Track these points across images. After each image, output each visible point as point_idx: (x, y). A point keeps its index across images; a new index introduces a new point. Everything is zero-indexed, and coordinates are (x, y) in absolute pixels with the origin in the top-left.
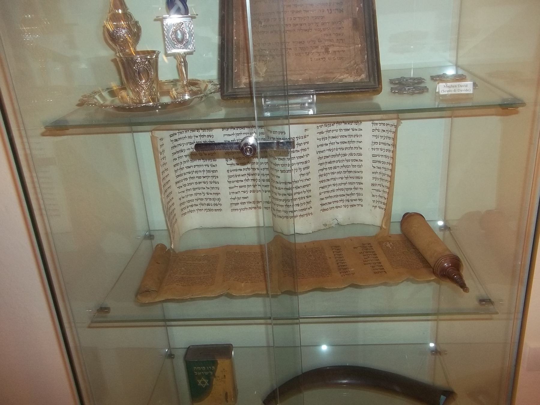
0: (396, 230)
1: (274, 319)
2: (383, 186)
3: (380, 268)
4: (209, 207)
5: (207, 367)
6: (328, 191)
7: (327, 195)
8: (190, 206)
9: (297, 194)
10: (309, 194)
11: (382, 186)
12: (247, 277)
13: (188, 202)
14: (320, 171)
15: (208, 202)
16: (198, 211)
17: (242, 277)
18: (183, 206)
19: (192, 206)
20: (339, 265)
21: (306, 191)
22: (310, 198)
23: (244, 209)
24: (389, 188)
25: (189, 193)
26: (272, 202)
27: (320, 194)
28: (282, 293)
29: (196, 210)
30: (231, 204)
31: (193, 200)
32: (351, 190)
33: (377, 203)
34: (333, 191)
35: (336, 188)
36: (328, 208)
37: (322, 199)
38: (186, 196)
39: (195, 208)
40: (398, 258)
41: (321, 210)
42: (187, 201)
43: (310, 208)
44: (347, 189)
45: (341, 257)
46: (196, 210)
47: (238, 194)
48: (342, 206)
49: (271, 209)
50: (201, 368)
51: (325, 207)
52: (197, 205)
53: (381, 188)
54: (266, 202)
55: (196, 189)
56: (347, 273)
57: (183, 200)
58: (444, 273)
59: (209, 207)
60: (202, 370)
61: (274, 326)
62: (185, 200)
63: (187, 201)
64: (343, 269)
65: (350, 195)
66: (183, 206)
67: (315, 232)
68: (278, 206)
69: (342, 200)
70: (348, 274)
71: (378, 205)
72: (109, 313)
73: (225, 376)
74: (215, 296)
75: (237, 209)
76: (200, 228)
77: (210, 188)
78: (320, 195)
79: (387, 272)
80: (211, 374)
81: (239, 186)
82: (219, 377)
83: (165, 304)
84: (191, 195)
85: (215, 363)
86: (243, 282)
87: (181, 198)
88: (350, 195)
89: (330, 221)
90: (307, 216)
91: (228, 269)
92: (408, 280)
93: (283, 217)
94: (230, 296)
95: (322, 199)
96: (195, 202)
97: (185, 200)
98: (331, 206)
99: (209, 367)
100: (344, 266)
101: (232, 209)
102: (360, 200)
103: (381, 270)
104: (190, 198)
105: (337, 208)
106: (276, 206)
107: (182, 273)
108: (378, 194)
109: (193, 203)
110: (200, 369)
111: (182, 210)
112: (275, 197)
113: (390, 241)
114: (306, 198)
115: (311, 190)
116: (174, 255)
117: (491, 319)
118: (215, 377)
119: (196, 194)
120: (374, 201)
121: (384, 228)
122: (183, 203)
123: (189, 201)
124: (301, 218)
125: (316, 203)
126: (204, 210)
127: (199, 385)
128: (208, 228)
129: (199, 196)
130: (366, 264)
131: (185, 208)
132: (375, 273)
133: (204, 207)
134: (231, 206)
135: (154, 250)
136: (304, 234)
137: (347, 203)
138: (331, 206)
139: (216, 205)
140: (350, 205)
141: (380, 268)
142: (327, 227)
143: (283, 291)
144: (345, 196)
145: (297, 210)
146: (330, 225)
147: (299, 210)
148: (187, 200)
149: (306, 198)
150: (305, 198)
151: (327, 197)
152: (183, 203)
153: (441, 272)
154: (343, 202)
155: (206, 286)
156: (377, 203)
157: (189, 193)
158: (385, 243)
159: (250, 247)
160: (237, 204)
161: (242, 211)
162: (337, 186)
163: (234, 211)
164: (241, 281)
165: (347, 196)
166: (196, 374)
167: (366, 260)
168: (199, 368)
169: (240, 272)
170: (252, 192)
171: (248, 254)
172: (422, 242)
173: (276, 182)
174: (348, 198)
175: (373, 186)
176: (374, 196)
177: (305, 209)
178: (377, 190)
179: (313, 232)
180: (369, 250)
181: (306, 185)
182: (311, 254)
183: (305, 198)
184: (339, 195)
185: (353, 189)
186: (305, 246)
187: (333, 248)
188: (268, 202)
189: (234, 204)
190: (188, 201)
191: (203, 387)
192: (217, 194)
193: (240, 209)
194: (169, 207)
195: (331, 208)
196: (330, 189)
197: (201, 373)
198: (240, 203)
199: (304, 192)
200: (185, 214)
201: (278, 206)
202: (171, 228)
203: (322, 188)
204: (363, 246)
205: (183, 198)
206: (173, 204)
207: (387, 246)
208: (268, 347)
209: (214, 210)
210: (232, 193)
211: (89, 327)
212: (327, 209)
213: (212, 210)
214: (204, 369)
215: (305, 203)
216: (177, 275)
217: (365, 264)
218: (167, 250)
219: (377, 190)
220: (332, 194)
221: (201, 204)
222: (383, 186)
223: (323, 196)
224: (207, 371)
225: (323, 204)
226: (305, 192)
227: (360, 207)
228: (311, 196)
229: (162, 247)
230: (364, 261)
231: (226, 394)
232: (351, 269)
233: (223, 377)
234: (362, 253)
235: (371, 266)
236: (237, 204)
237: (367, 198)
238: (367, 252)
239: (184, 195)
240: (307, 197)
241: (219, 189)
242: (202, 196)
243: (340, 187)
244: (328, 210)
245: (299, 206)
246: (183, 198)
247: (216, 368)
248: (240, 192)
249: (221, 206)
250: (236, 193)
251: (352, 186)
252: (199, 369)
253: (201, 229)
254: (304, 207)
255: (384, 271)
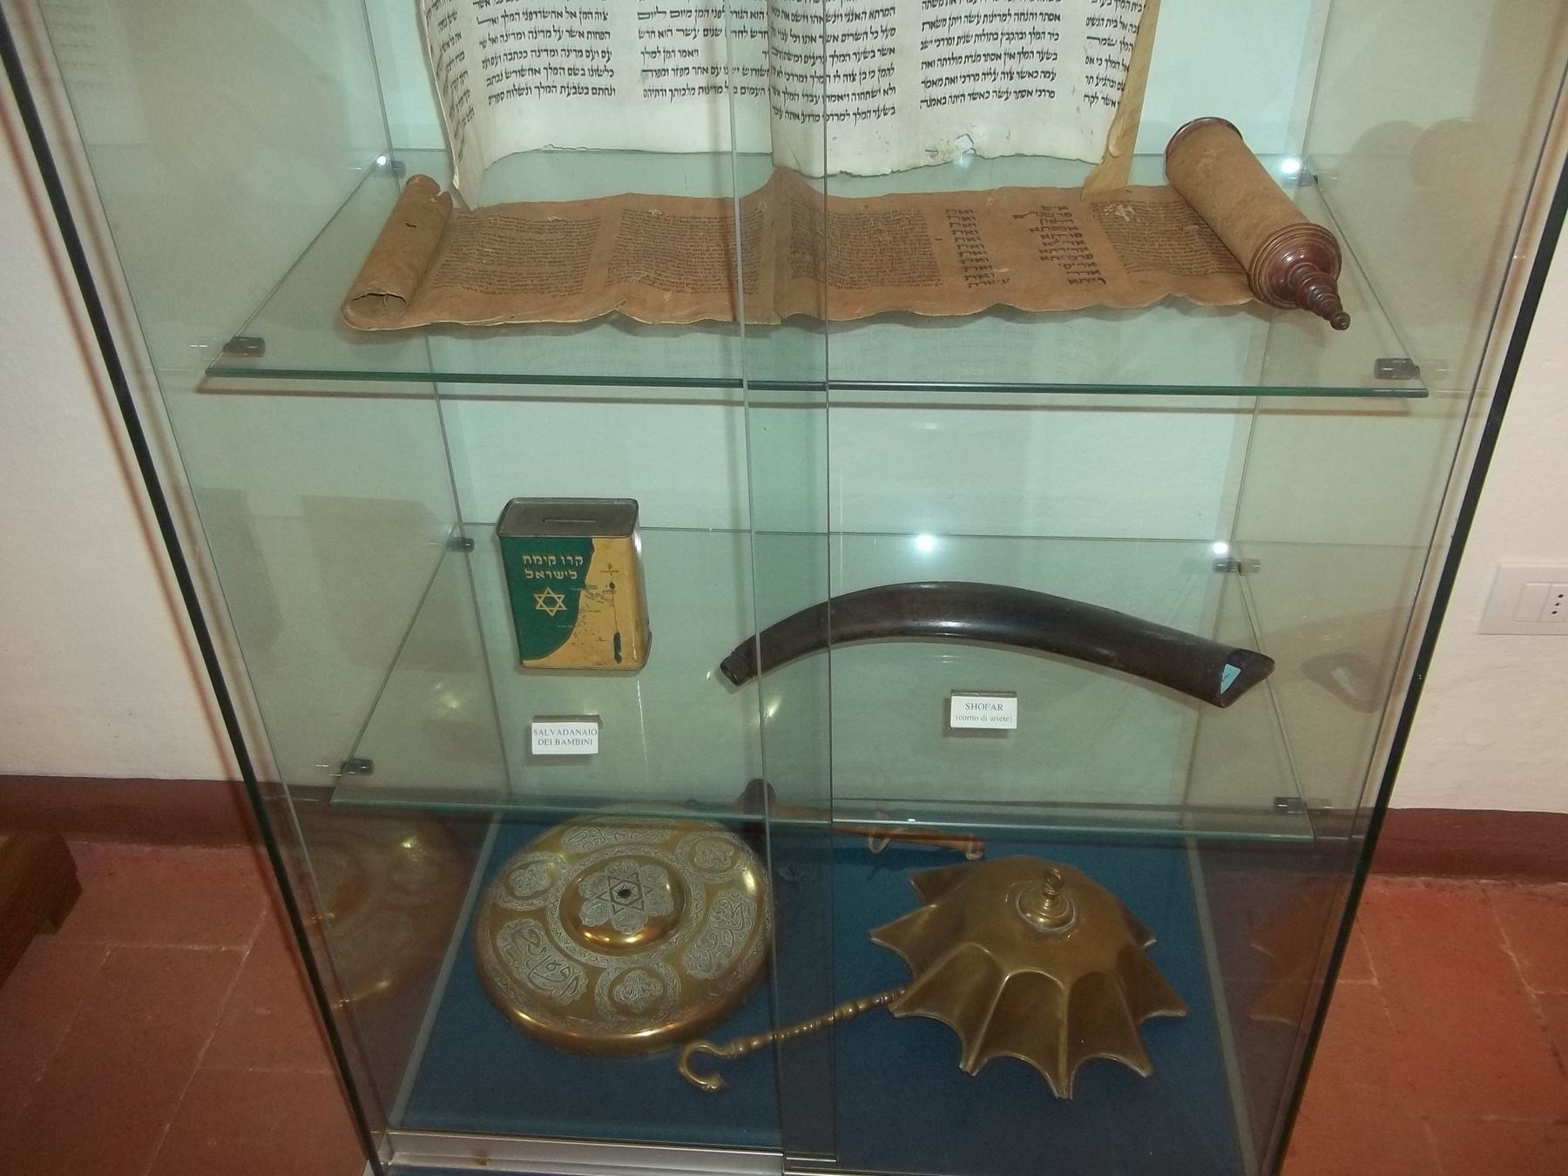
0: (1148, 174)
1: (754, 386)
2: (1124, 26)
3: (1087, 269)
4: (575, 80)
5: (563, 558)
6: (950, 38)
7: (945, 51)
8: (515, 72)
9: (851, 37)
10: (888, 43)
11: (1119, 25)
12: (680, 279)
13: (509, 57)
14: (927, 26)
15: (573, 61)
16: (542, 90)
17: (666, 277)
18: (493, 70)
19: (521, 72)
20: (963, 258)
21: (880, 31)
22: (889, 58)
23: (683, 92)
24: (1122, 87)
25: (514, 26)
26: (774, 71)
27: (924, 45)
28: (782, 320)
29: (536, 87)
30: (643, 71)
31: (524, 54)
32: (1022, 38)
33: (1101, 84)
34: (965, 38)
35: (974, 29)
36: (945, 98)
37: (929, 64)
38: (502, 36)
39: (532, 81)
40: (1147, 247)
41: (922, 102)
42: (505, 55)
43: (890, 92)
44: (1010, 36)
45: (973, 239)
46: (536, 87)
47: (665, 38)
48: (991, 92)
49: (767, 92)
50: (545, 558)
51: (936, 92)
52: (536, 71)
53: (1116, 34)
54: (755, 70)
55: (534, 16)
56: (985, 279)
57: (491, 50)
58: (1282, 281)
59: (575, 80)
60: (545, 566)
61: (752, 411)
62: (501, 48)
63: (505, 55)
64: (976, 270)
65: (1017, 56)
66: (493, 70)
67: (899, 171)
68: (788, 80)
69: (992, 71)
70: (989, 282)
71: (1101, 92)
72: (260, 356)
73: (612, 585)
74: (581, 320)
75: (662, 90)
76: (547, 148)
77: (578, 14)
78: (922, 49)
79: (1107, 282)
80: (573, 578)
81: (671, 12)
82: (595, 587)
83: (435, 341)
84: (520, 34)
85: (587, 550)
86: (668, 290)
87: (485, 41)
88: (1017, 56)
89: (948, 142)
90: (879, 117)
91: (624, 253)
92: (1169, 302)
93: (803, 115)
94: (626, 325)
95: (929, 64)
96: (530, 62)
97: (501, 48)
98: (955, 89)
99: (570, 558)
100: (977, 260)
101: (645, 90)
102: (1046, 73)
103: (1091, 276)
104: (514, 45)
105: (974, 99)
106: (783, 79)
107: (484, 261)
108: (1105, 52)
109: (526, 63)
110: (541, 563)
111: (490, 81)
112: (780, 49)
113: (1128, 202)
114: (877, 54)
115: (894, 29)
116: (462, 215)
117: (1405, 413)
118: (584, 586)
119: (534, 33)
120: (1092, 77)
121: (1112, 155)
122: (493, 60)
123: (512, 56)
124: (860, 122)
125: (909, 78)
126: (559, 90)
127: (538, 608)
128: (573, 151)
129: (542, 41)
130: (1047, 258)
131: (498, 78)
132: (1071, 282)
133: (562, 79)
134: (644, 80)
135: (402, 191)
136: (865, 177)
137: (1004, 84)
138: (955, 89)
139: (596, 72)
140: (1015, 92)
141: (1087, 269)
142: (939, 159)
143: (786, 316)
144: (1003, 59)
145: (848, 95)
146: (949, 153)
147: (853, 94)
148: (507, 52)
149: (877, 54)
150: (874, 56)
151: (945, 59)
152: (493, 60)
153: (1271, 277)
154: (995, 79)
155: (555, 296)
156: (1101, 84)
157: (514, 26)
158: (1111, 206)
159: (697, 203)
160: (661, 72)
161: (677, 97)
162: (978, 22)
163: (653, 96)
164: (663, 287)
165: (1007, 59)
166: (530, 575)
167: (1048, 248)
168: (539, 558)
169: (662, 263)
170: (710, 35)
171: (690, 220)
172: (1221, 205)
173: (783, 12)
174: (1013, 65)
175: (1093, 25)
176: (1092, 61)
177: (873, 94)
178: (1107, 42)
179: (892, 172)
180: (1058, 224)
181: (882, 11)
182: (880, 227)
183: (874, 56)
184: (984, 55)
185: (1028, 36)
186: (866, 207)
187: (951, 213)
188: (759, 72)
189: (654, 73)
190: (510, 54)
191: (550, 616)
192: (602, 35)
193: (671, 90)
194: (446, 60)
195: (955, 96)
196: (958, 30)
197: (545, 574)
198: (673, 70)
199: (872, 33)
200: (498, 97)
201: (788, 80)
202: (450, 121)
203: (932, 25)
204: (1044, 212)
205: (494, 41)
206: (461, 56)
207: (1117, 213)
208: (737, 532)
209: (590, 92)
210: (648, 32)
211: (201, 390)
212: (943, 101)
213: (585, 91)
214: (552, 561)
215: (874, 72)
216: (469, 264)
217: (1042, 259)
218: (439, 194)
219: (1107, 42)
220: (962, 50)
221: (551, 69)
222: (1124, 26)
223: (933, 53)
224: (559, 566)
225: (930, 81)
226: (875, 35)
227: (1045, 98)
228: (892, 51)
229: (425, 185)
230: (1041, 252)
231: (617, 638)
232: (999, 269)
233: (609, 588)
234: (1037, 229)
235: (1060, 265)
236: (661, 72)
237: (1072, 72)
238: (1055, 229)
239: (496, 30)
240: (883, 52)
241: (605, 18)
242: (552, 43)
243: (989, 27)
244: (945, 103)
245: (854, 79)
246: (494, 41)
247: (587, 560)
248: (671, 31)
249: (611, 76)
250: (661, 34)
251: (1027, 27)
252: (538, 560)
253: (551, 152)
254: (869, 84)
255: (1100, 279)
